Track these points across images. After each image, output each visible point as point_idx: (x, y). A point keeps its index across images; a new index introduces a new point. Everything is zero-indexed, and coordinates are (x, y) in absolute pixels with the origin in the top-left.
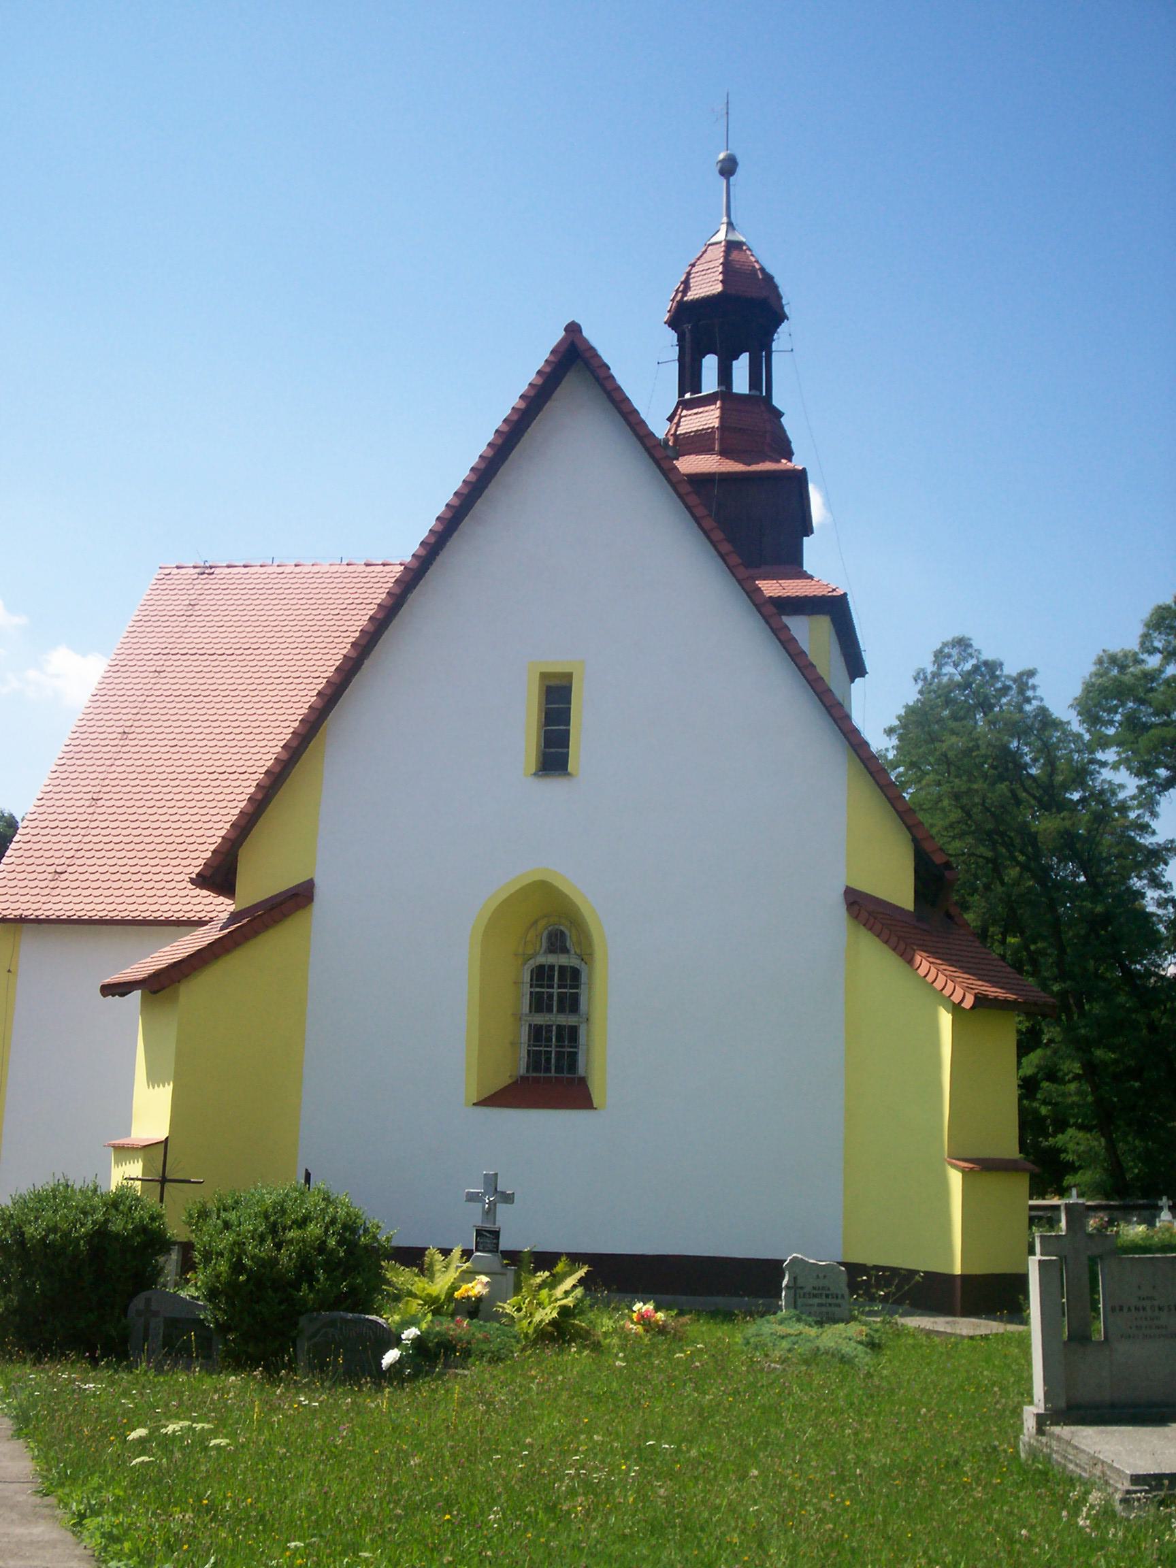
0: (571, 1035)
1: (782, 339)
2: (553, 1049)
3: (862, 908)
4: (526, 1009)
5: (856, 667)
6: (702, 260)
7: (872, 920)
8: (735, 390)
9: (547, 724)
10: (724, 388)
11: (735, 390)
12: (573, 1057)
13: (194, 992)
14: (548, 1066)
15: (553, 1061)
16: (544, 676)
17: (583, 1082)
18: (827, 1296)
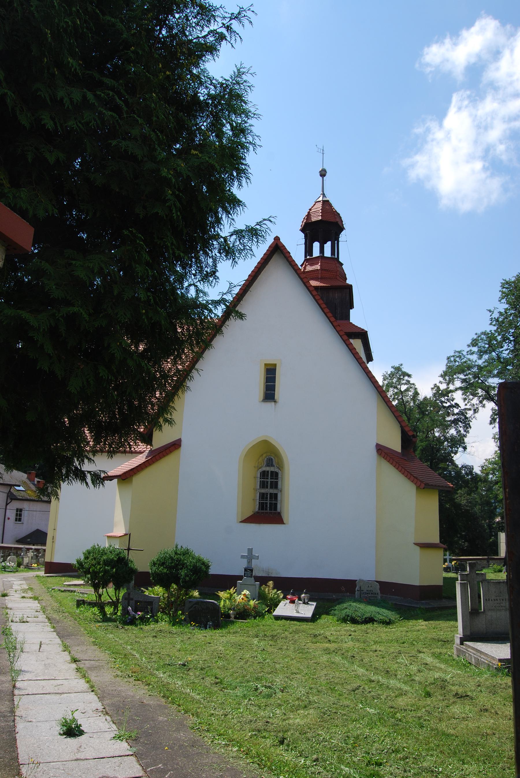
0: (275, 497)
1: (343, 236)
2: (268, 502)
3: (382, 451)
4: (258, 487)
5: (370, 358)
6: (314, 208)
7: (386, 456)
8: (325, 255)
9: (266, 383)
10: (321, 255)
11: (325, 255)
12: (276, 504)
13: (137, 479)
14: (267, 509)
15: (268, 506)
16: (266, 365)
17: (279, 514)
18: (372, 594)
